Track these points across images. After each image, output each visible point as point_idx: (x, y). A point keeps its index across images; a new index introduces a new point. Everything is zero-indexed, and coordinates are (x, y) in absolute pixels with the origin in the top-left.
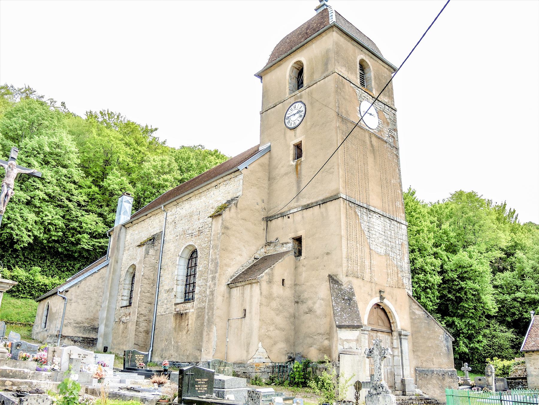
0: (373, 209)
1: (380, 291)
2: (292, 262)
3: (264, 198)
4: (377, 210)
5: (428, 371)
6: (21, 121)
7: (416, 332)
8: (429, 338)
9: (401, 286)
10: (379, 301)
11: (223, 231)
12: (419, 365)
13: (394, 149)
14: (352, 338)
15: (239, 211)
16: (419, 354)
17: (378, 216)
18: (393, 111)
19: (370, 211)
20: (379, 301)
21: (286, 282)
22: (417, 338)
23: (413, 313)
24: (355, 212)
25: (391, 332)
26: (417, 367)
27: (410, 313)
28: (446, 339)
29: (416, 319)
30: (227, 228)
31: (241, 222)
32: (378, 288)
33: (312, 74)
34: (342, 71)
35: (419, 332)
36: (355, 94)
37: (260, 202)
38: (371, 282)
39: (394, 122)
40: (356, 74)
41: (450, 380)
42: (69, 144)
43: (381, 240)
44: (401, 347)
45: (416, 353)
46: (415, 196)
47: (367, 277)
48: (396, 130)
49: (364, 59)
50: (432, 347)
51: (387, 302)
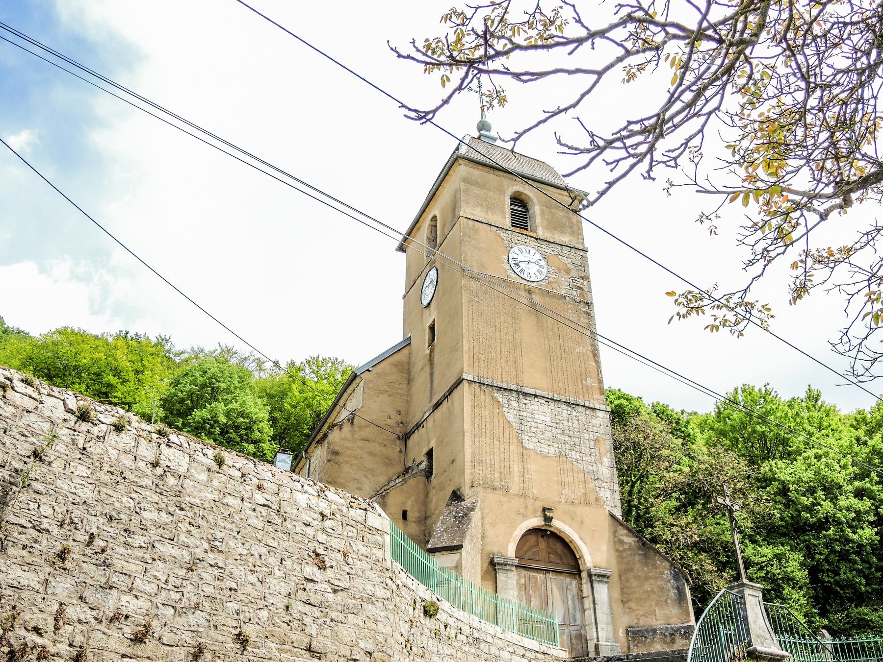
0: (527, 390)
1: (544, 509)
2: (421, 486)
3: (400, 408)
4: (539, 393)
5: (646, 630)
6: (188, 388)
7: (625, 572)
8: (647, 578)
9: (591, 501)
10: (543, 523)
11: (329, 457)
12: (633, 623)
13: (582, 305)
14: (449, 565)
15: (356, 428)
16: (633, 605)
17: (543, 401)
18: (581, 253)
19: (525, 394)
20: (543, 523)
21: (409, 515)
22: (627, 581)
23: (621, 542)
24: (493, 398)
25: (579, 572)
26: (631, 627)
27: (614, 542)
28: (674, 577)
29: (624, 550)
30: (336, 453)
31: (360, 443)
32: (539, 505)
33: (444, 226)
34: (475, 213)
35: (631, 570)
36: (499, 240)
37: (393, 414)
38: (524, 496)
39: (584, 266)
40: (504, 213)
41: (684, 641)
42: (260, 411)
43: (549, 435)
44: (593, 595)
45: (627, 605)
46: (821, 399)
47: (514, 489)
48: (586, 278)
49: (521, 190)
50: (653, 591)
51: (558, 524)
